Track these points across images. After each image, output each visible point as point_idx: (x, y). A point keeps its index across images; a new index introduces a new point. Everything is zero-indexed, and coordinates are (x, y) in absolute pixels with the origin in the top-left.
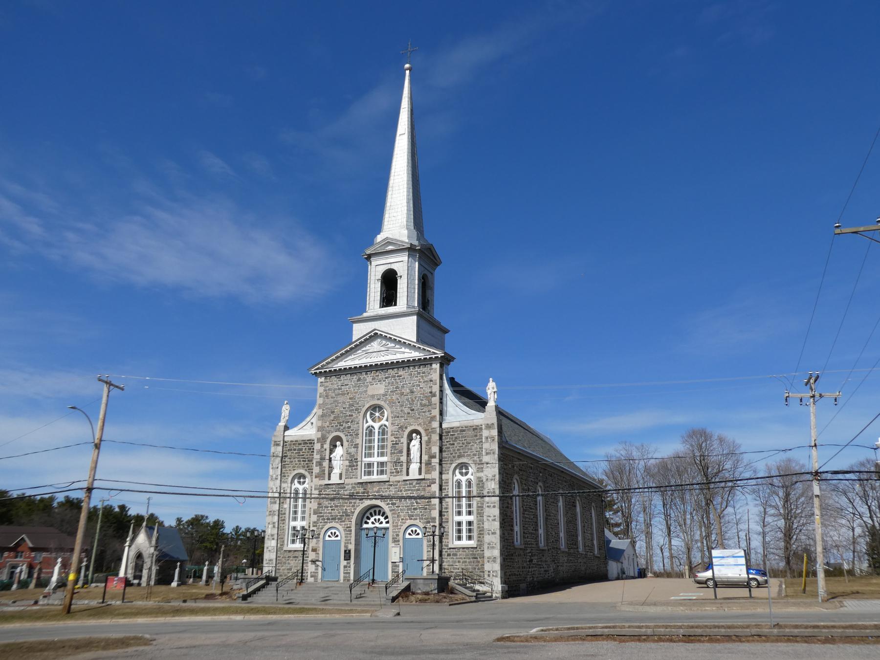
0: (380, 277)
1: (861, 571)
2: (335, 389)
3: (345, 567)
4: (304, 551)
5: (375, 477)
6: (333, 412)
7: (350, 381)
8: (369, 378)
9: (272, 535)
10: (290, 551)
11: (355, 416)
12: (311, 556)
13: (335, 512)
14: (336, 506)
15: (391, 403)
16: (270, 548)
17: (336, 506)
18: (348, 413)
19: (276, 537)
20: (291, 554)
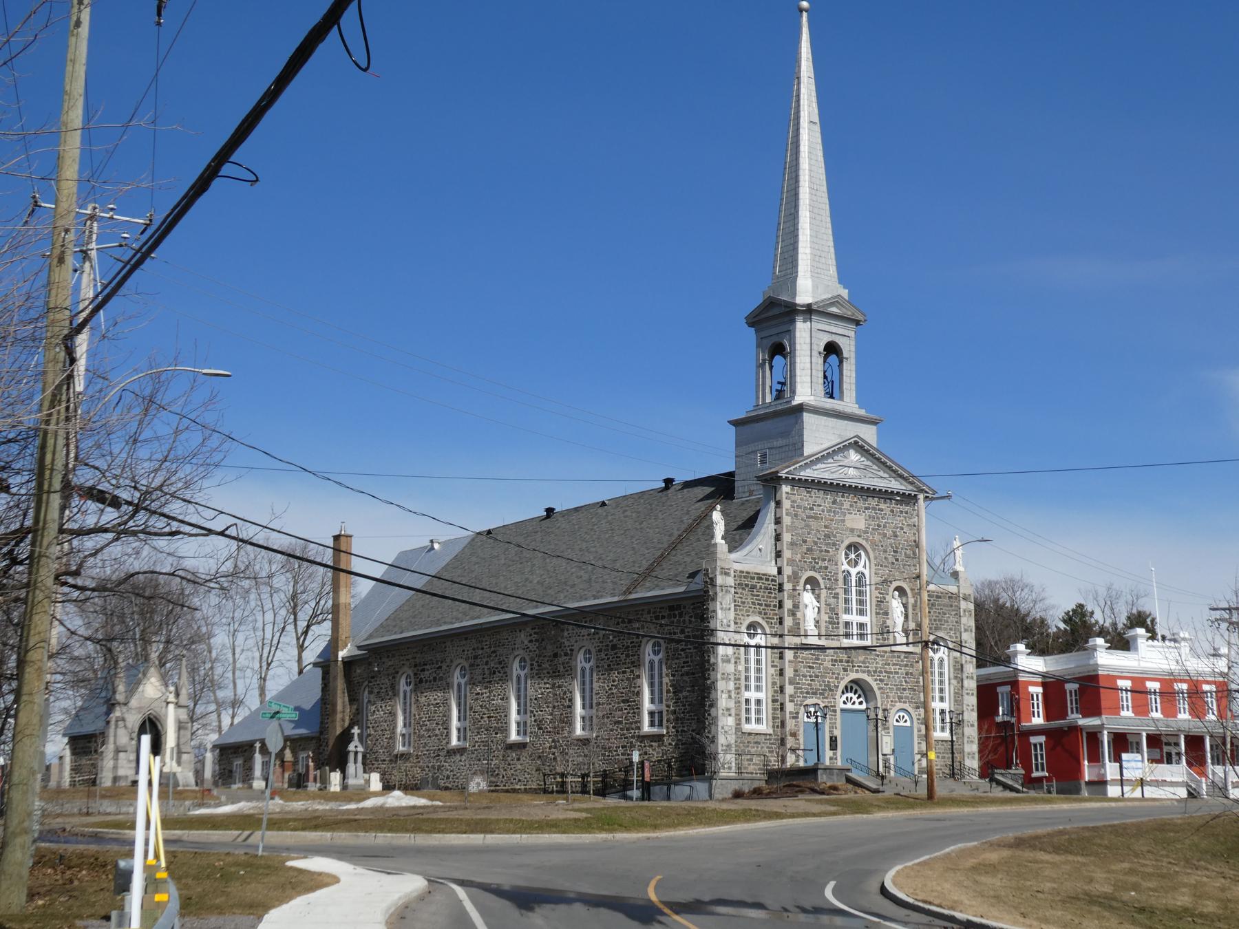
0: (822, 349)
1: (116, 779)
2: (805, 508)
3: (831, 759)
4: (952, 741)
5: (855, 642)
6: (805, 541)
7: (823, 501)
8: (846, 501)
9: (728, 710)
10: (750, 734)
11: (832, 553)
12: (790, 742)
13: (817, 684)
14: (817, 676)
15: (874, 545)
16: (726, 728)
17: (817, 676)
18: (824, 548)
19: (733, 712)
20: (751, 739)
